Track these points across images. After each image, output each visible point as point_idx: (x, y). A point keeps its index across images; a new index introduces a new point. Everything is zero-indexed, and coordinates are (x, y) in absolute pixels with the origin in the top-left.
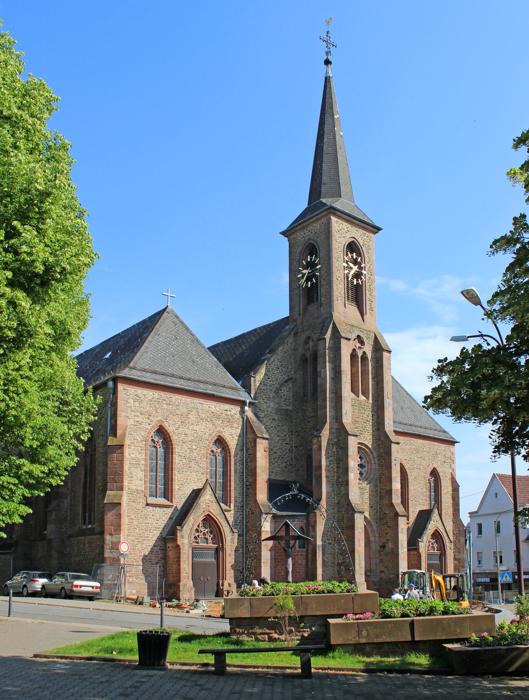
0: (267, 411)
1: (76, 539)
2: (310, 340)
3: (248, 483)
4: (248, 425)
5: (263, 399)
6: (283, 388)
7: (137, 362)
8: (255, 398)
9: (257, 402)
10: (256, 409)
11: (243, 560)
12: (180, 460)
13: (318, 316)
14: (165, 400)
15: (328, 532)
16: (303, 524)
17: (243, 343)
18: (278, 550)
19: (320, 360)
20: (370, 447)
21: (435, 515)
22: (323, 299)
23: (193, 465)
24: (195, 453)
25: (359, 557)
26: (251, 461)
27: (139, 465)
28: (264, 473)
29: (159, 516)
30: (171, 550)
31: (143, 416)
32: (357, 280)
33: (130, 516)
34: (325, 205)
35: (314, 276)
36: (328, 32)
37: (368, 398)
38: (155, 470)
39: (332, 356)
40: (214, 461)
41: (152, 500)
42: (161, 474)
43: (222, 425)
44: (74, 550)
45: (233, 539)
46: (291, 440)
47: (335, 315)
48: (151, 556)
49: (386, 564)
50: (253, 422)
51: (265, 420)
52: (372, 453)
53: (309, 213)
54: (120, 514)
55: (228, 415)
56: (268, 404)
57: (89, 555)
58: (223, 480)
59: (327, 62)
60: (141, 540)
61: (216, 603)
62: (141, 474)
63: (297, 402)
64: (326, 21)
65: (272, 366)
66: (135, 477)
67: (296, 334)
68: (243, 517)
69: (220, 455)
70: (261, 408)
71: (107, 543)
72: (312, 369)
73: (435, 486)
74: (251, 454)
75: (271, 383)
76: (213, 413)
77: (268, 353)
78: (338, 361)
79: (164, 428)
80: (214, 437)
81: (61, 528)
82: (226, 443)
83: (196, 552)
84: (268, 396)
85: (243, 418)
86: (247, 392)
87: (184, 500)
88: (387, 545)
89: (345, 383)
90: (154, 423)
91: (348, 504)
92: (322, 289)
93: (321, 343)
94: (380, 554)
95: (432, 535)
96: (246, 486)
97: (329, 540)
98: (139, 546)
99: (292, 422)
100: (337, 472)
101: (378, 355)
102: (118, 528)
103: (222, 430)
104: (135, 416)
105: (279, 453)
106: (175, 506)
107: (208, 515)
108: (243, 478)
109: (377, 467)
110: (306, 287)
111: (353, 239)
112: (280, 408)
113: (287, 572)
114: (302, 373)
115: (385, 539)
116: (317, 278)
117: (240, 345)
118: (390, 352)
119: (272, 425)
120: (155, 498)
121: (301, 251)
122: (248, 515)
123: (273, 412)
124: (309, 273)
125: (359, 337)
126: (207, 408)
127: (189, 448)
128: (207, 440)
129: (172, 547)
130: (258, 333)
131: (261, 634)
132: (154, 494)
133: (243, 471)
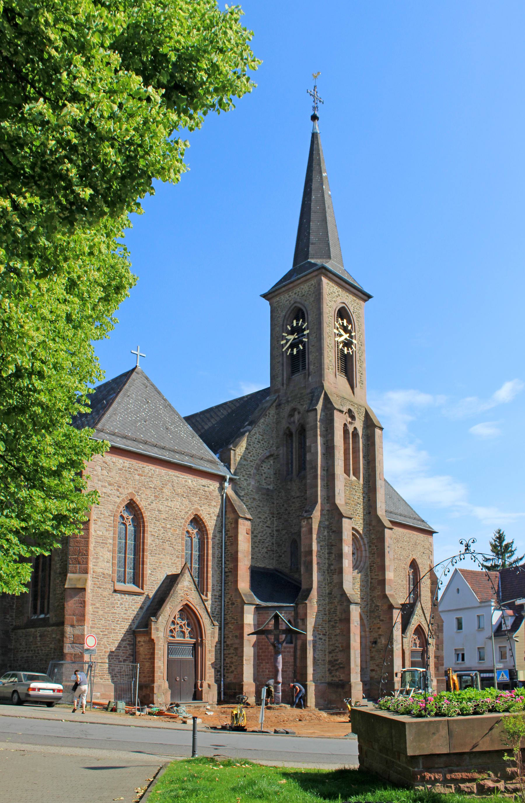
0: (248, 489)
1: (23, 631)
2: (296, 413)
3: (227, 570)
4: (227, 503)
5: (243, 476)
6: (264, 465)
7: (104, 425)
8: (235, 474)
9: (238, 477)
10: (235, 486)
11: (221, 657)
12: (153, 541)
13: (305, 387)
14: (136, 470)
15: (319, 625)
16: (291, 617)
17: (212, 417)
18: (262, 645)
19: (309, 434)
20: (361, 532)
21: (418, 608)
22: (312, 367)
23: (167, 547)
24: (169, 533)
25: (355, 653)
26: (232, 544)
27: (106, 544)
28: (246, 559)
29: (129, 605)
30: (142, 645)
31: (112, 487)
32: (348, 350)
33: (94, 605)
34: (315, 265)
35: (302, 342)
36: (315, 87)
37: (358, 478)
38: (123, 551)
39: (323, 429)
40: (190, 544)
41: (120, 586)
42: (130, 556)
43: (199, 502)
44: (21, 644)
45: (213, 633)
46: (272, 523)
47: (326, 385)
48: (118, 652)
49: (378, 662)
50: (233, 501)
51: (245, 499)
52: (362, 538)
53: (295, 274)
54: (84, 602)
55: (206, 491)
56: (248, 482)
57: (42, 650)
58: (199, 565)
59: (314, 118)
60: (106, 633)
61: (195, 707)
62: (108, 555)
63: (279, 481)
64: (313, 75)
65: (253, 439)
66: (102, 559)
67: (279, 405)
68: (221, 609)
69: (196, 537)
70: (242, 486)
71: (68, 636)
72: (297, 444)
73: (413, 579)
74: (231, 537)
75: (252, 458)
76: (190, 488)
77: (249, 425)
78: (330, 435)
79: (134, 502)
80: (190, 515)
81: (5, 618)
82: (203, 523)
83: (172, 647)
84: (248, 473)
85: (222, 496)
86: (226, 466)
87: (156, 587)
88: (379, 640)
89: (338, 459)
90: (124, 496)
91: (342, 595)
92: (310, 356)
93: (311, 414)
94: (370, 650)
95: (415, 631)
96: (225, 572)
97: (320, 634)
98: (105, 640)
99: (273, 503)
100: (328, 559)
101: (369, 432)
102: (82, 618)
103: (200, 508)
104: (102, 486)
105: (259, 538)
106: (146, 593)
107: (187, 605)
108: (222, 564)
109: (368, 555)
110: (291, 354)
111: (344, 305)
112: (260, 486)
113: (277, 671)
114: (285, 448)
115: (377, 634)
116: (305, 344)
117: (208, 419)
118: (381, 429)
119: (253, 505)
120: (123, 584)
121: (285, 316)
122: (227, 605)
123: (254, 491)
124: (294, 339)
125: (350, 411)
126: (184, 482)
127: (163, 527)
128: (183, 518)
129: (144, 642)
130: (229, 407)
131: (464, 781)
132: (123, 579)
133: (222, 556)
